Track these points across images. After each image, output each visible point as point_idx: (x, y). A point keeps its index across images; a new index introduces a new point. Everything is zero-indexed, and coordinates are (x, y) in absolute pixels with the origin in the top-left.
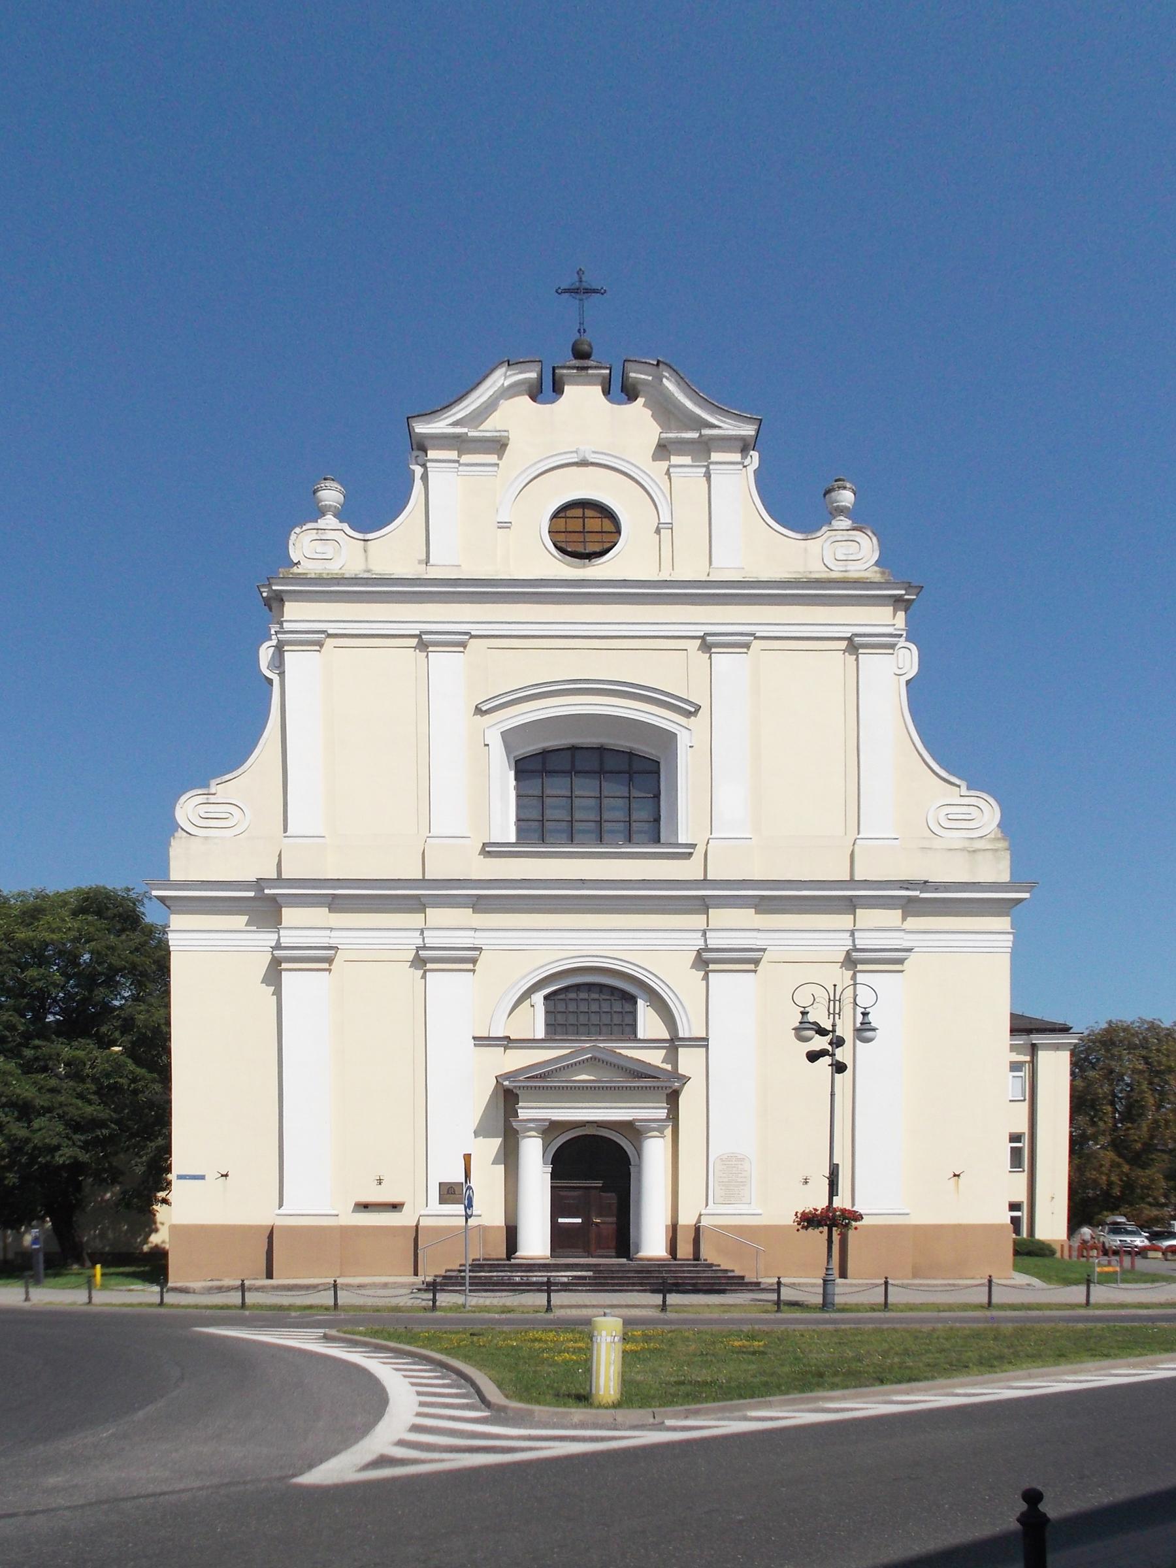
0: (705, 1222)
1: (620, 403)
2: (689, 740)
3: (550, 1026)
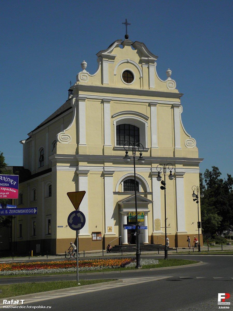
0: (154, 235)
1: (134, 50)
2: (147, 125)
3: (125, 189)
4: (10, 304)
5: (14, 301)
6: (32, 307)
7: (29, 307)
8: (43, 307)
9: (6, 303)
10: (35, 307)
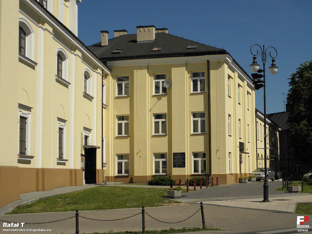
4: (10, 227)
5: (14, 224)
6: (32, 230)
7: (29, 230)
8: (43, 230)
9: (6, 226)
10: (36, 230)
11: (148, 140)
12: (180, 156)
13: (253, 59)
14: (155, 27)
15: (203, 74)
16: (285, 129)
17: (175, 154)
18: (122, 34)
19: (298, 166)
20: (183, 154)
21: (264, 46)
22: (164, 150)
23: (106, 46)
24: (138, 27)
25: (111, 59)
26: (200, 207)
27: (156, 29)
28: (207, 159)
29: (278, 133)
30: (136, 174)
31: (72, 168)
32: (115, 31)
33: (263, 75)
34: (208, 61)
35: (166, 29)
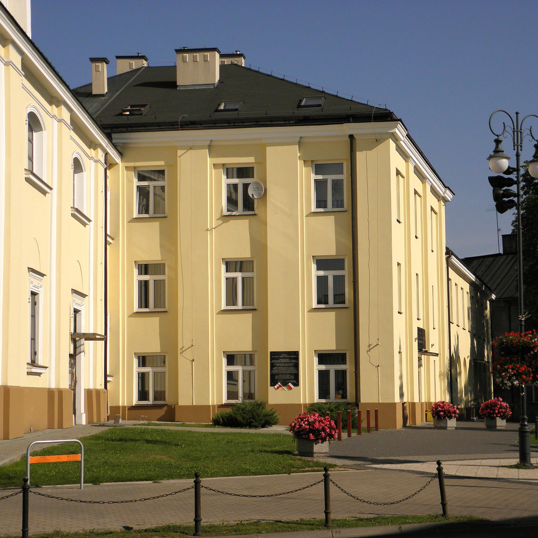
11: (212, 321)
12: (287, 361)
13: (494, 145)
14: (219, 52)
15: (337, 168)
16: (502, 295)
17: (275, 355)
18: (135, 64)
19: (337, 372)
20: (294, 356)
21: (517, 113)
22: (244, 344)
23: (103, 95)
24: (178, 51)
25: (122, 129)
26: (194, 484)
27: (222, 56)
28: (348, 367)
29: (488, 302)
30: (183, 401)
31: (53, 386)
32: (118, 57)
33: (515, 179)
34: (351, 137)
35: (241, 55)
